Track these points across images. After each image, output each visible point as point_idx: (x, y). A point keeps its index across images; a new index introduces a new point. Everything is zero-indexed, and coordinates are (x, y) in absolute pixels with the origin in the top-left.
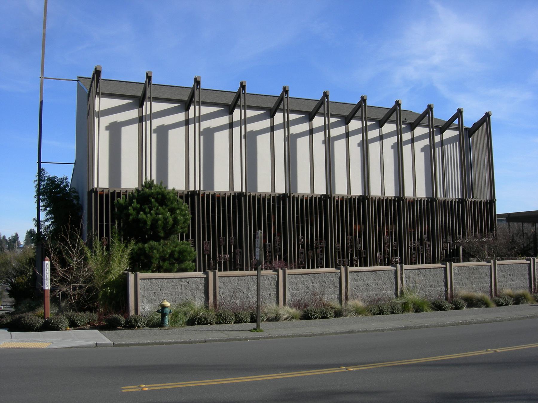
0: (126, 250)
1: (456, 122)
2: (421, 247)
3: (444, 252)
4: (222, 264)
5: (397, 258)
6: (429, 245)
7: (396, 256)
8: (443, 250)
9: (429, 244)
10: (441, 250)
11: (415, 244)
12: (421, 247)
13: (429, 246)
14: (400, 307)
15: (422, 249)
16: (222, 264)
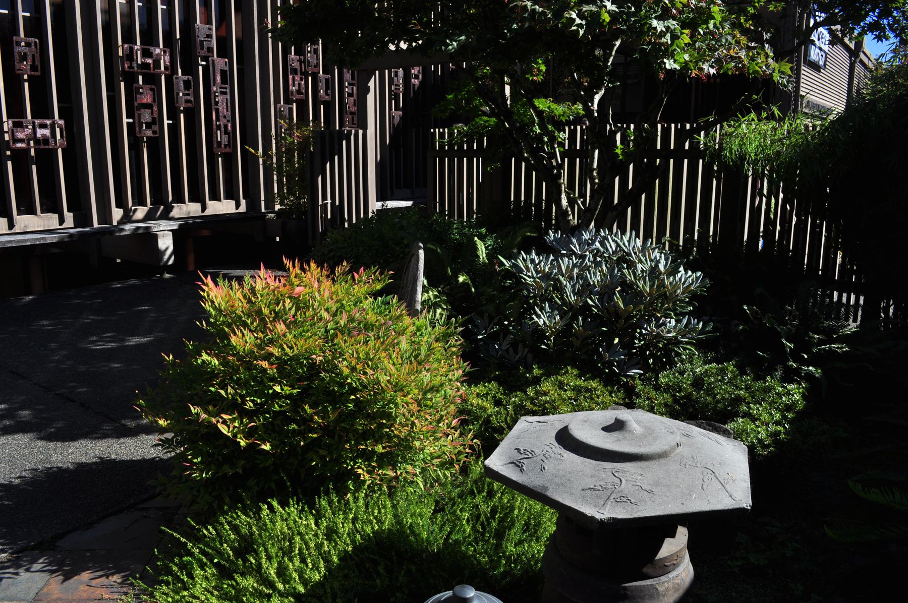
0: (20, 418)
2: (186, 78)
3: (291, 110)
4: (806, 256)
5: (43, 126)
6: (223, 73)
7: (42, 110)
8: (288, 101)
9: (227, 68)
10: (277, 101)
11: (150, 61)
12: (186, 78)
13: (226, 77)
14: (362, 492)
15: (191, 90)
16: (806, 256)
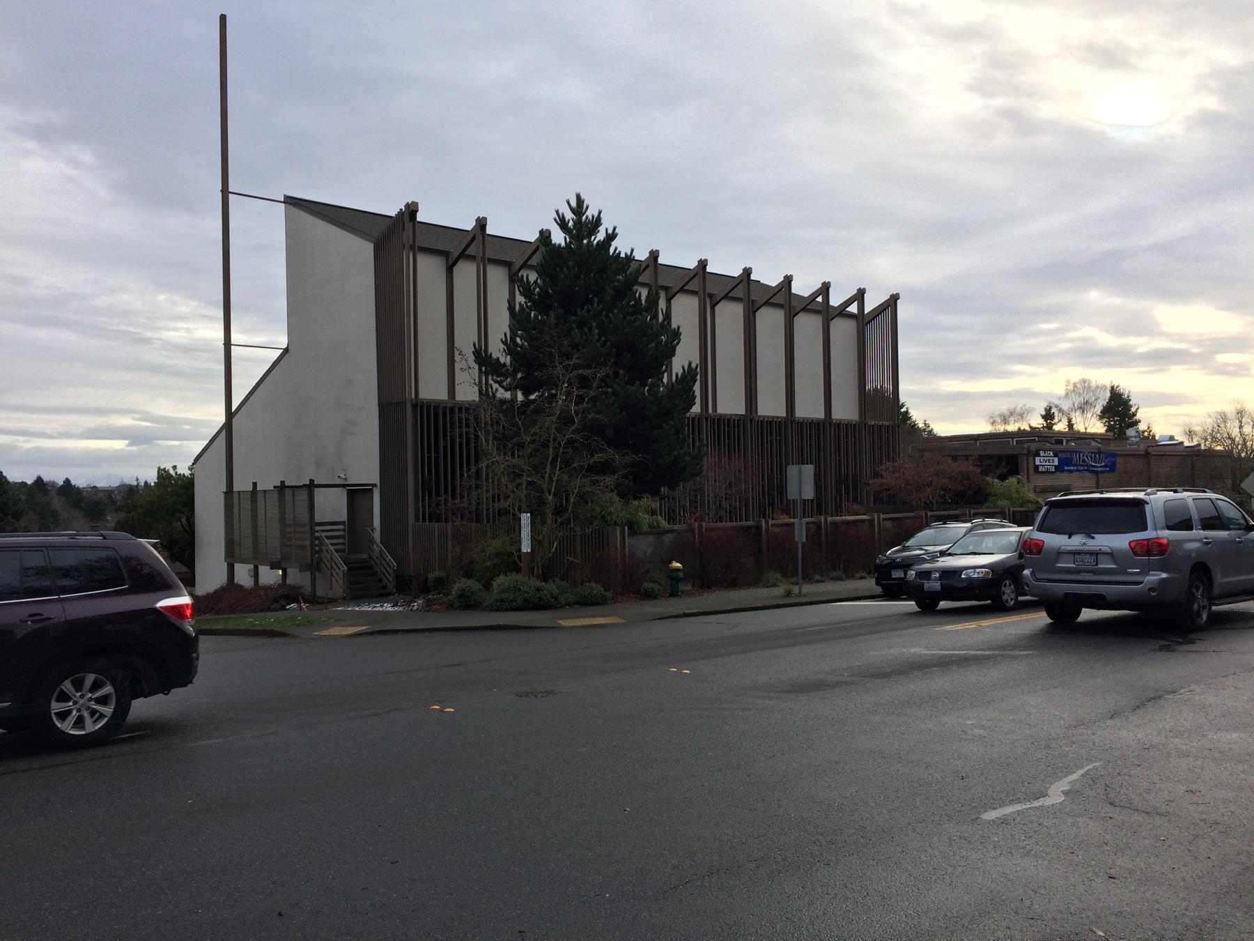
1: (820, 299)
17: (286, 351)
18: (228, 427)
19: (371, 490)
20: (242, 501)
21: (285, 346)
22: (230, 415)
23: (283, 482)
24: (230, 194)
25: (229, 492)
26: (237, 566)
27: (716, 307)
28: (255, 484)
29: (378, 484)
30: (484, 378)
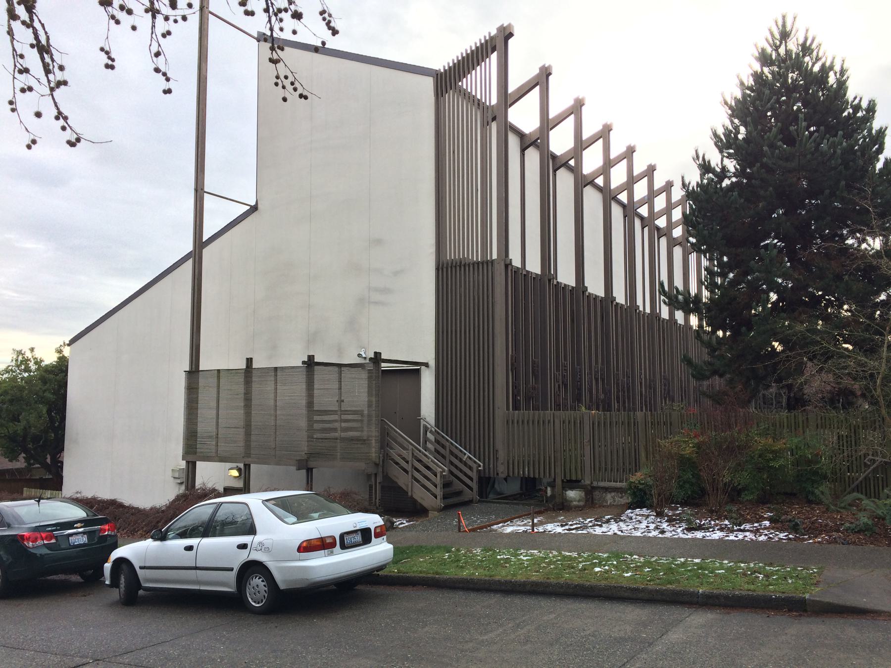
17: (254, 209)
18: (196, 256)
19: (418, 372)
20: (215, 405)
21: (253, 203)
22: (200, 244)
23: (311, 358)
24: (205, 194)
25: (194, 373)
26: (200, 465)
27: (660, 239)
28: (249, 361)
29: (432, 363)
30: (466, 256)
